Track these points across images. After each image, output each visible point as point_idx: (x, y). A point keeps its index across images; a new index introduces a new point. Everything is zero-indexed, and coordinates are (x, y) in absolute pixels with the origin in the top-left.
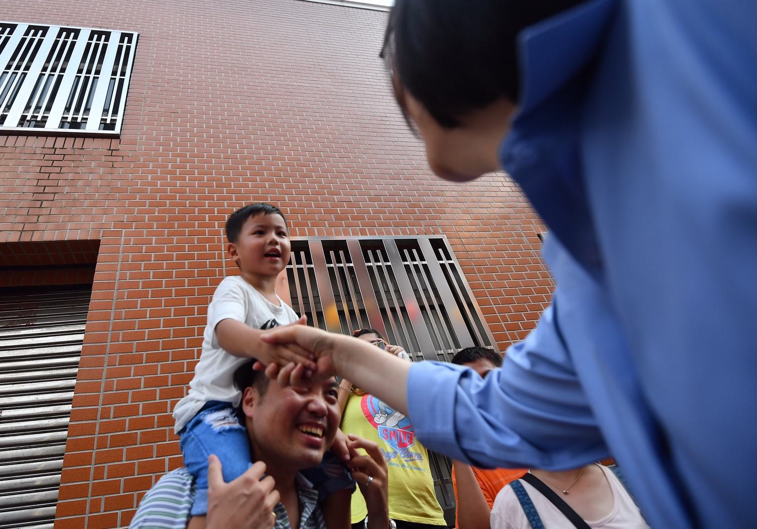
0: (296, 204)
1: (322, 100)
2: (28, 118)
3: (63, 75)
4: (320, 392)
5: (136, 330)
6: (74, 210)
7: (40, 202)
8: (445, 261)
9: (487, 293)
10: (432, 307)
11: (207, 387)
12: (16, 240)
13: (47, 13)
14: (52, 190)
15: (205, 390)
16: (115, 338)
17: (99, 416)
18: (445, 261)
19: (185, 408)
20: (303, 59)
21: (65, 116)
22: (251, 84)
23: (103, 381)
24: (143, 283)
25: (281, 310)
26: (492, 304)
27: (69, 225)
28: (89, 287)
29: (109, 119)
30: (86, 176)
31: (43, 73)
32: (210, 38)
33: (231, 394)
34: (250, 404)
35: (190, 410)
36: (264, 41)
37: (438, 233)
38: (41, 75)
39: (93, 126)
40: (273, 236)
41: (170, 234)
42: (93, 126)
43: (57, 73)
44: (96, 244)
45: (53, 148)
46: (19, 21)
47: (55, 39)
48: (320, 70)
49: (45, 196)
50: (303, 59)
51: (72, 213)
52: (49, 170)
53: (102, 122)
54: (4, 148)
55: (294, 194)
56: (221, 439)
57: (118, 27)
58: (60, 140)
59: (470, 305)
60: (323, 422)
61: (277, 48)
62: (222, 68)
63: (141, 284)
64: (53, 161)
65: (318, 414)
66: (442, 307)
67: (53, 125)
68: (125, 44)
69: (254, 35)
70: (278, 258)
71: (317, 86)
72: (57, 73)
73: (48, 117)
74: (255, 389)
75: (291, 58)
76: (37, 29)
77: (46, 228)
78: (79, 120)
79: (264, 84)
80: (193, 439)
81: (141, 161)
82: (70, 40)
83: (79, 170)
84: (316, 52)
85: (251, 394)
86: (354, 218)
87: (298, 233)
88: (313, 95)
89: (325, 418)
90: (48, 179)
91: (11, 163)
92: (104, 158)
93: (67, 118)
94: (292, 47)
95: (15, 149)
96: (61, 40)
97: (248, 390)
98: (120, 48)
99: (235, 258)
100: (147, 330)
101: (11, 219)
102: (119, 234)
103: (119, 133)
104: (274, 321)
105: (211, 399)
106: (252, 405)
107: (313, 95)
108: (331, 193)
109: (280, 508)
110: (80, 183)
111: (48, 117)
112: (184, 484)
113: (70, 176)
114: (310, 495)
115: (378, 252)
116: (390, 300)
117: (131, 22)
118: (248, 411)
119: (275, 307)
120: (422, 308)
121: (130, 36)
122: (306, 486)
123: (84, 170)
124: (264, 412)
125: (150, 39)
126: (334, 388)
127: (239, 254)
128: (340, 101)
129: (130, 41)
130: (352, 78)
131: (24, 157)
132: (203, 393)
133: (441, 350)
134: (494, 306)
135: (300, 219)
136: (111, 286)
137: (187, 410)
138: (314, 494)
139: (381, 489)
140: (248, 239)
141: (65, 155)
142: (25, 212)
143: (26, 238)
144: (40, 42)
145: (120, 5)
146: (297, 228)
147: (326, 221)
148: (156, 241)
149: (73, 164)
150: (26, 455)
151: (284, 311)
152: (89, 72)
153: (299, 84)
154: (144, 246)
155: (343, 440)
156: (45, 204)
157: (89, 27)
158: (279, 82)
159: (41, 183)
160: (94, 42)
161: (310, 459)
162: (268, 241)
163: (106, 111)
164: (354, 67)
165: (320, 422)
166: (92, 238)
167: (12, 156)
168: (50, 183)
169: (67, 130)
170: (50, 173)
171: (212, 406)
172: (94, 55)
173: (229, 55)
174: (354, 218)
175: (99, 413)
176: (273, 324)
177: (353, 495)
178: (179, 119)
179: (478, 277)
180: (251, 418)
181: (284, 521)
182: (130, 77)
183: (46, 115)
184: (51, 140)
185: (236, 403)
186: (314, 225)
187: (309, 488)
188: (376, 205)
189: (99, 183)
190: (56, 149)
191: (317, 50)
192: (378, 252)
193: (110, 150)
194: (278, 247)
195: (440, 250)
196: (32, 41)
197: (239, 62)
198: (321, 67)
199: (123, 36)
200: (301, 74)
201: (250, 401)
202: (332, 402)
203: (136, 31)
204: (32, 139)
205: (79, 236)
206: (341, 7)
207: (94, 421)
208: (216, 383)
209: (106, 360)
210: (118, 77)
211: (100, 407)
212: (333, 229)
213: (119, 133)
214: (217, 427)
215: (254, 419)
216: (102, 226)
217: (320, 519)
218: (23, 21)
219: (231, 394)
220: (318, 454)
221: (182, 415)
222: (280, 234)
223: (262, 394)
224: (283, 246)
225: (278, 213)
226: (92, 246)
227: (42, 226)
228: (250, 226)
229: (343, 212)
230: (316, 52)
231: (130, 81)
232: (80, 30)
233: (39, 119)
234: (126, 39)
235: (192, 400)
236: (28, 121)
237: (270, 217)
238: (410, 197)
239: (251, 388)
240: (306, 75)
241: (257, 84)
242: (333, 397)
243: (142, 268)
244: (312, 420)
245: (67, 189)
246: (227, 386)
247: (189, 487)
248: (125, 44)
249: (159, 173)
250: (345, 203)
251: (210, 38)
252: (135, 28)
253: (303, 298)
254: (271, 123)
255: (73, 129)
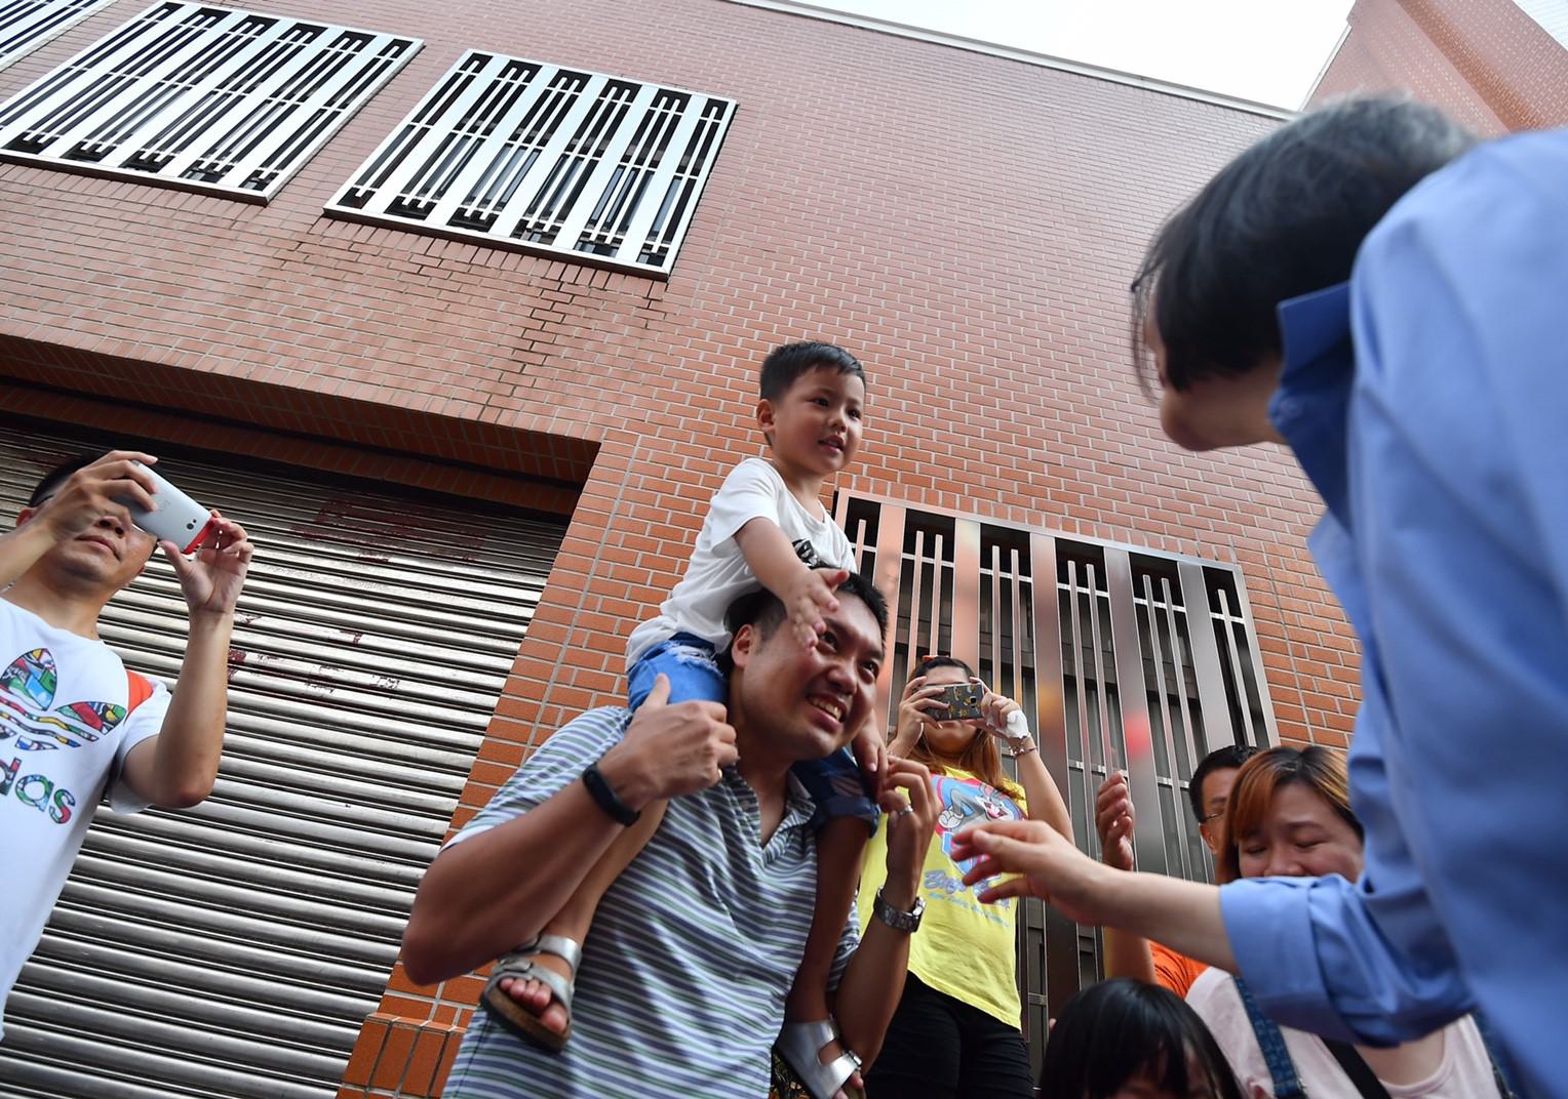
0: (950, 449)
1: (1050, 264)
2: (530, 226)
3: (597, 162)
4: (853, 659)
5: (625, 600)
6: (570, 388)
7: (522, 365)
8: (1225, 616)
9: (1301, 697)
10: (1174, 701)
11: (684, 613)
12: (474, 418)
13: (592, 50)
14: (544, 348)
15: (680, 617)
16: (589, 605)
17: (538, 718)
18: (1225, 616)
19: (646, 633)
20: (1031, 183)
21: (588, 230)
22: (919, 217)
23: (557, 666)
24: (653, 527)
25: (823, 529)
26: (1307, 720)
27: (558, 410)
28: (565, 521)
29: (657, 245)
30: (600, 336)
31: (567, 153)
32: (863, 125)
33: (717, 632)
34: (746, 650)
35: (652, 637)
36: (964, 141)
37: (1228, 559)
38: (564, 157)
39: (628, 254)
40: (842, 415)
41: (714, 458)
42: (628, 254)
43: (588, 157)
44: (593, 448)
45: (559, 280)
46: (545, 60)
47: (597, 97)
48: (1061, 207)
49: (530, 357)
50: (1031, 183)
51: (567, 392)
52: (546, 315)
53: (644, 251)
54: (484, 269)
55: (951, 429)
56: (685, 670)
57: (706, 88)
58: (573, 269)
59: (1258, 717)
60: (846, 701)
61: (985, 156)
62: (873, 181)
63: (649, 527)
64: (555, 302)
65: (843, 687)
66: (1195, 705)
67: (565, 243)
68: (710, 120)
69: (948, 127)
70: (838, 450)
71: (1047, 237)
72: (588, 157)
73: (560, 228)
74: (758, 630)
75: (1008, 178)
76: (571, 76)
77: (522, 407)
78: (608, 241)
79: (944, 221)
80: (646, 668)
81: (695, 325)
82: (621, 103)
83: (592, 324)
84: (1062, 172)
85: (749, 635)
86: (1057, 497)
87: (940, 501)
88: (1035, 254)
89: (851, 697)
90: (541, 330)
91: (490, 294)
92: (634, 311)
93: (589, 235)
94: (1016, 157)
95: (499, 272)
96: (607, 100)
97: (747, 628)
98: (701, 125)
99: (767, 427)
100: (642, 604)
101: (474, 383)
102: (632, 440)
103: (668, 272)
104: (808, 543)
105: (684, 630)
106: (747, 652)
107: (1035, 254)
108: (1024, 443)
109: (750, 796)
110: (589, 345)
111: (560, 228)
112: (618, 719)
113: (576, 331)
114: (803, 807)
115: (1090, 568)
116: (1089, 665)
117: (729, 82)
118: (738, 657)
119: (815, 522)
120: (1153, 697)
121: (722, 106)
122: (799, 794)
123: (600, 325)
124: (762, 664)
125: (755, 115)
126: (876, 661)
127: (775, 424)
128: (1087, 272)
129: (719, 116)
130: (1123, 232)
131: (511, 287)
132: (676, 621)
133: (1169, 777)
134: (1309, 727)
135: (951, 478)
136: (600, 521)
137: (648, 637)
138: (809, 807)
139: (918, 833)
140: (796, 408)
141: (574, 295)
142: (496, 375)
143: (489, 417)
144: (573, 99)
145: (717, 48)
146: (941, 492)
147: (1000, 492)
148: (688, 464)
149: (583, 312)
150: (419, 756)
151: (828, 531)
152: (640, 161)
153: (1012, 229)
154: (668, 468)
155: (875, 744)
156: (528, 369)
157: (657, 82)
158: (974, 221)
159: (529, 334)
160: (659, 110)
161: (815, 743)
162: (831, 421)
163: (653, 234)
164: (1134, 210)
165: (842, 700)
166: (587, 439)
167: (493, 283)
168: (543, 337)
169: (588, 255)
170: (545, 321)
171: (683, 638)
172: (655, 132)
173: (890, 159)
174: (1057, 497)
175: (540, 713)
176: (805, 547)
177: (886, 872)
178: (774, 263)
179: (1290, 663)
180: (741, 669)
181: (753, 816)
182: (708, 178)
183: (557, 225)
184: (558, 267)
185: (721, 647)
186: (973, 493)
187: (804, 798)
188: (1110, 481)
189: (619, 350)
190: (563, 282)
191: (1067, 168)
192: (1090, 568)
193: (647, 298)
194: (843, 436)
195: (1222, 593)
196: (560, 96)
197: (907, 175)
198: (1064, 202)
199: (711, 103)
200: (1022, 212)
201: (744, 646)
202: (867, 680)
203: (734, 97)
204: (529, 260)
205: (569, 430)
206: (1137, 90)
207: (529, 724)
208: (699, 608)
209: (569, 635)
210: (686, 176)
211: (543, 705)
212: (1009, 507)
213: (668, 272)
214: (682, 658)
215: (745, 672)
216: (607, 422)
217: (810, 847)
218: (552, 61)
219: (717, 632)
220: (829, 741)
221: (639, 643)
222: (853, 413)
223: (764, 639)
224: (850, 435)
225: (859, 375)
226: (586, 452)
227: (517, 403)
228: (806, 384)
229: (1037, 481)
230: (1062, 172)
231: (705, 185)
232: (640, 86)
233: (546, 229)
234: (715, 110)
235: (658, 625)
236: (529, 230)
237: (846, 380)
238: (1186, 480)
239: (750, 627)
240: (1032, 214)
241: (932, 219)
242: (870, 673)
243: (657, 504)
244: (830, 693)
245: (566, 352)
246: (715, 620)
247: (622, 722)
248: (710, 120)
249: (719, 351)
250: (1046, 465)
251: (863, 125)
252: (733, 93)
253: (919, 620)
254: (939, 296)
255: (596, 259)
